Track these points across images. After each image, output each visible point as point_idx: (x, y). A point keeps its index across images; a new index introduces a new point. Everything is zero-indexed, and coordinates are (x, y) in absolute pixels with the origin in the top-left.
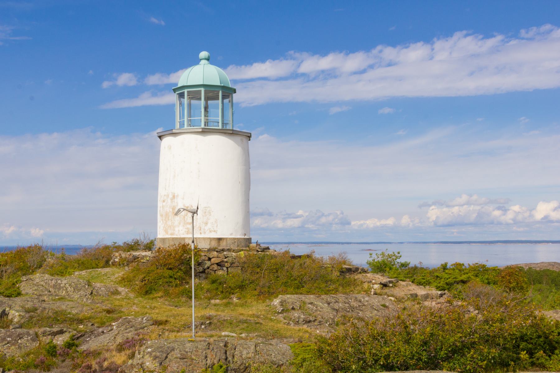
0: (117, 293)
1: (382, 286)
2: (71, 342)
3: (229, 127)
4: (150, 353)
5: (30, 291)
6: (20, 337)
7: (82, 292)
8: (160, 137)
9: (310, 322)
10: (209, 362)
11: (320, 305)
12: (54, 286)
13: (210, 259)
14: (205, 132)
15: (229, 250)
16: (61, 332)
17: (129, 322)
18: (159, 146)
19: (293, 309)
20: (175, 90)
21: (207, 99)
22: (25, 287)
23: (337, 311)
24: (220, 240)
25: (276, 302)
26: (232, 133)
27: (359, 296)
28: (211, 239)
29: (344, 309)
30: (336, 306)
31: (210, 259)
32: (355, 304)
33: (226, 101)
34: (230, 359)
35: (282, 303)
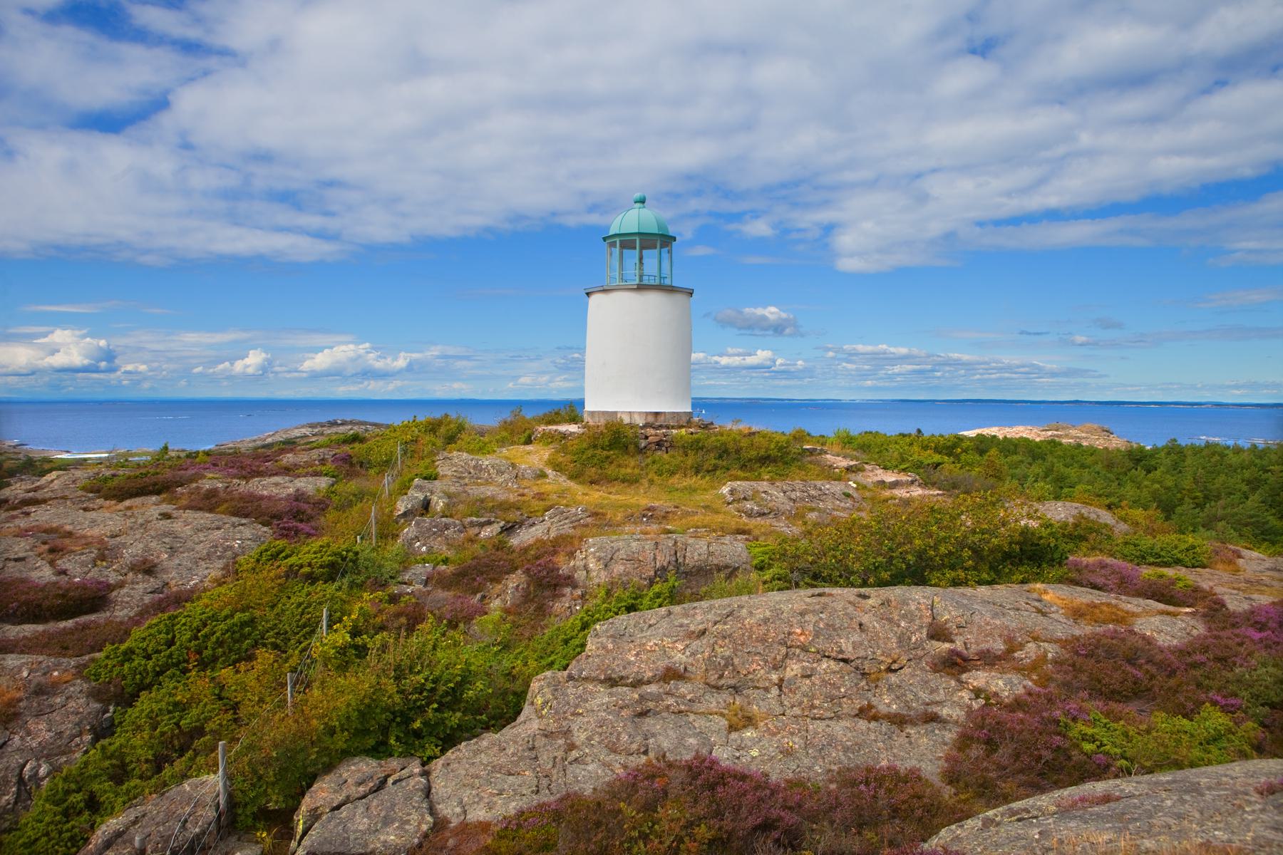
0: (543, 475)
1: (218, 41)
2: (355, 460)
3: (667, 282)
4: (594, 553)
5: (449, 473)
6: (447, 527)
7: (506, 476)
8: (588, 294)
9: (764, 514)
10: (658, 565)
11: (773, 491)
12: (475, 467)
13: (647, 438)
14: (641, 288)
15: (668, 427)
16: (489, 523)
17: (562, 513)
18: (587, 304)
19: (745, 499)
20: (605, 239)
21: (642, 248)
22: (444, 469)
23: (794, 501)
24: (657, 414)
25: (725, 490)
26: (671, 289)
27: (819, 483)
28: (647, 414)
29: (802, 499)
30: (793, 496)
31: (647, 438)
32: (813, 492)
33: (665, 250)
34: (680, 560)
35: (732, 492)
